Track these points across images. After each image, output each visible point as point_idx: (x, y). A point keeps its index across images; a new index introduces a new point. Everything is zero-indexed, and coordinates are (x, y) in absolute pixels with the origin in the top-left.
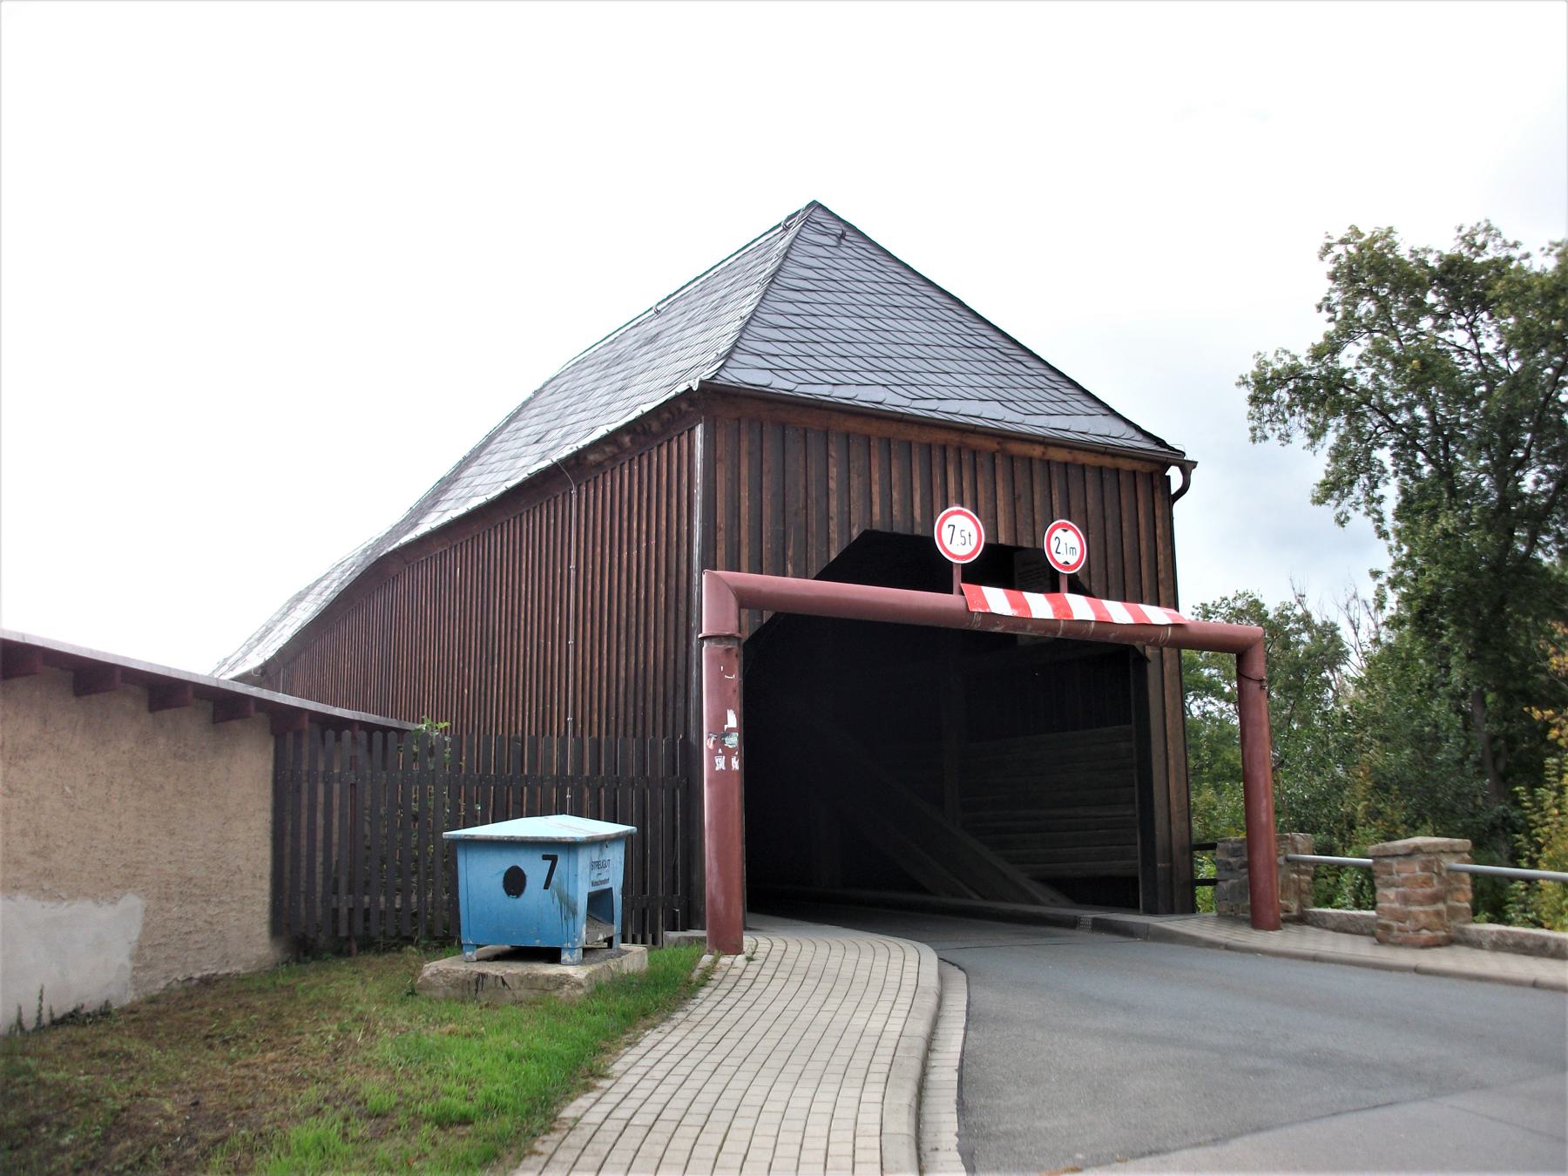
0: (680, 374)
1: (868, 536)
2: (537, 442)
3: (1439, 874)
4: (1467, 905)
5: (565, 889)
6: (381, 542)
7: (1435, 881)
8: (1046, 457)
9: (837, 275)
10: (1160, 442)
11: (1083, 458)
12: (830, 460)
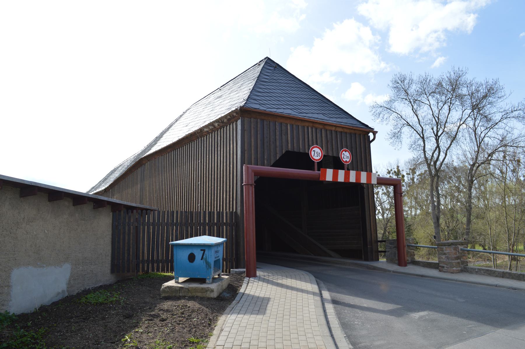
0: (232, 106)
1: (287, 152)
2: (186, 126)
3: (458, 251)
5: (208, 260)
6: (139, 155)
7: (457, 253)
8: (336, 130)
9: (275, 78)
10: (367, 126)
11: (346, 130)
12: (277, 130)
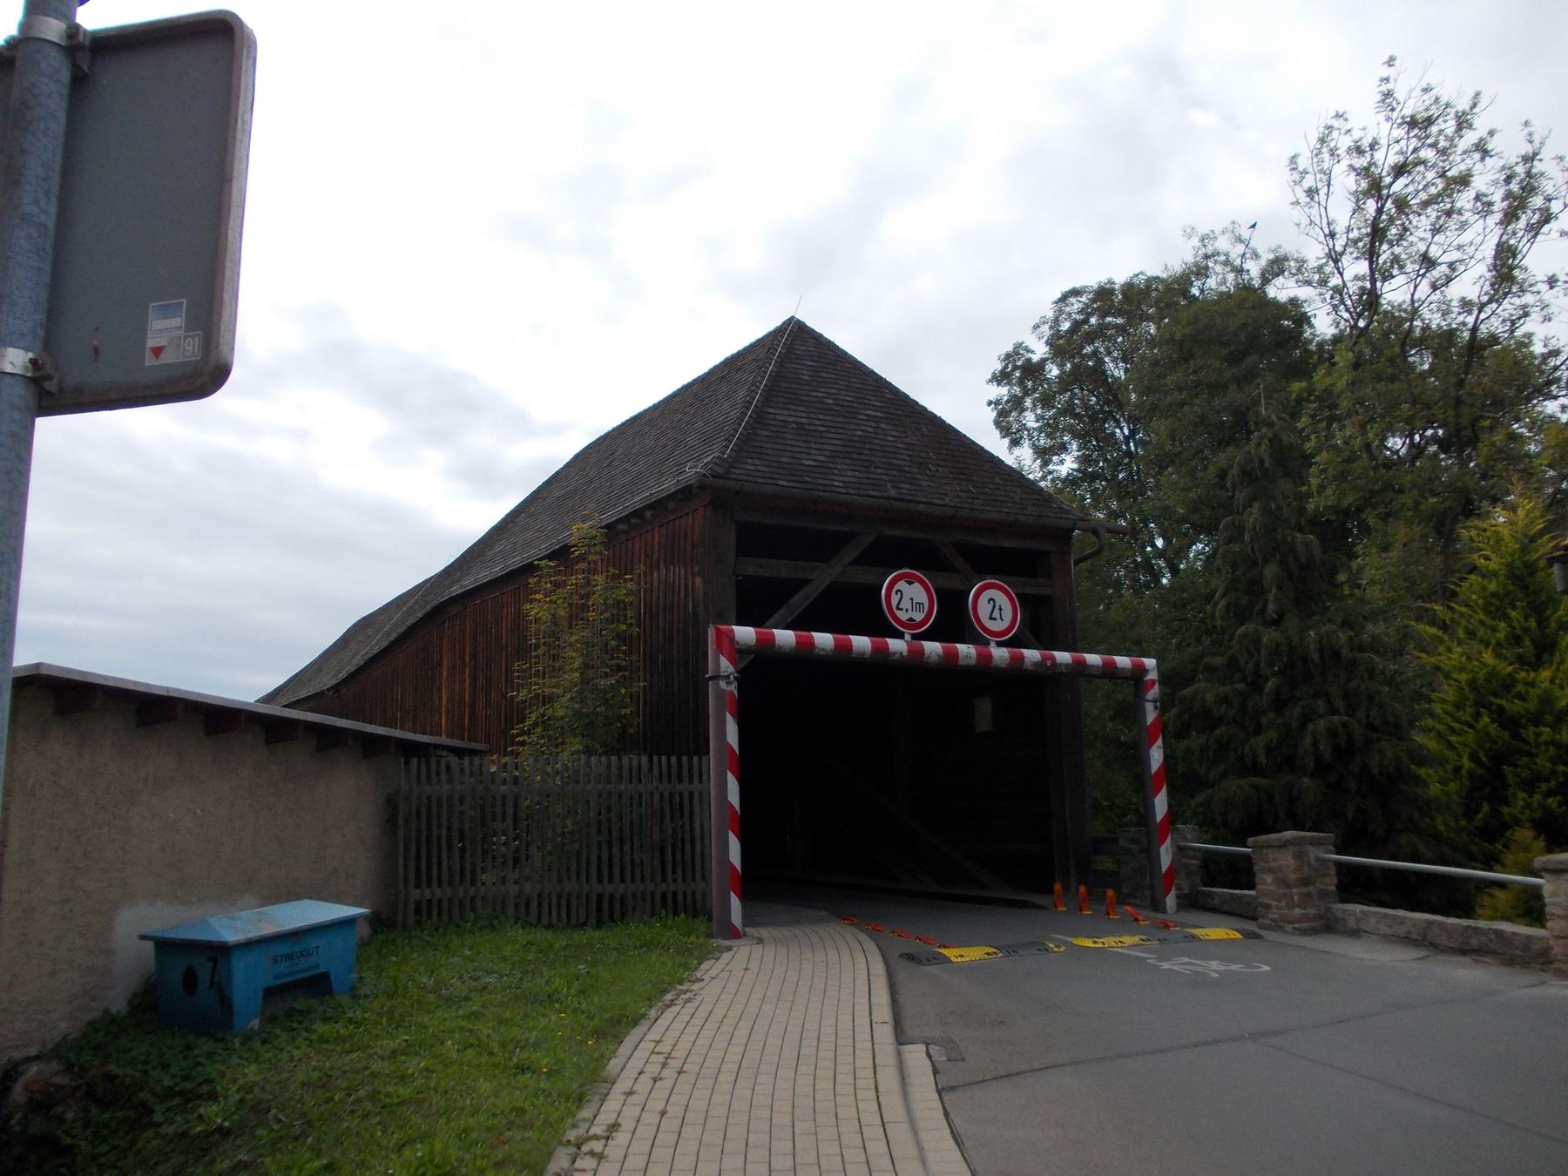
4: (1334, 888)
